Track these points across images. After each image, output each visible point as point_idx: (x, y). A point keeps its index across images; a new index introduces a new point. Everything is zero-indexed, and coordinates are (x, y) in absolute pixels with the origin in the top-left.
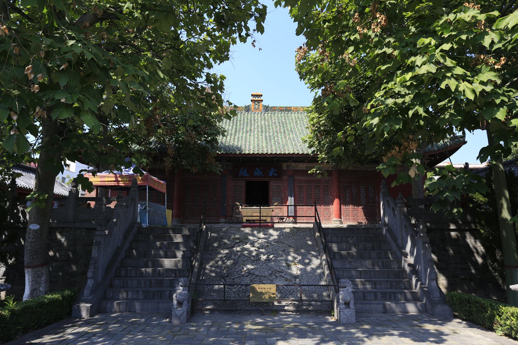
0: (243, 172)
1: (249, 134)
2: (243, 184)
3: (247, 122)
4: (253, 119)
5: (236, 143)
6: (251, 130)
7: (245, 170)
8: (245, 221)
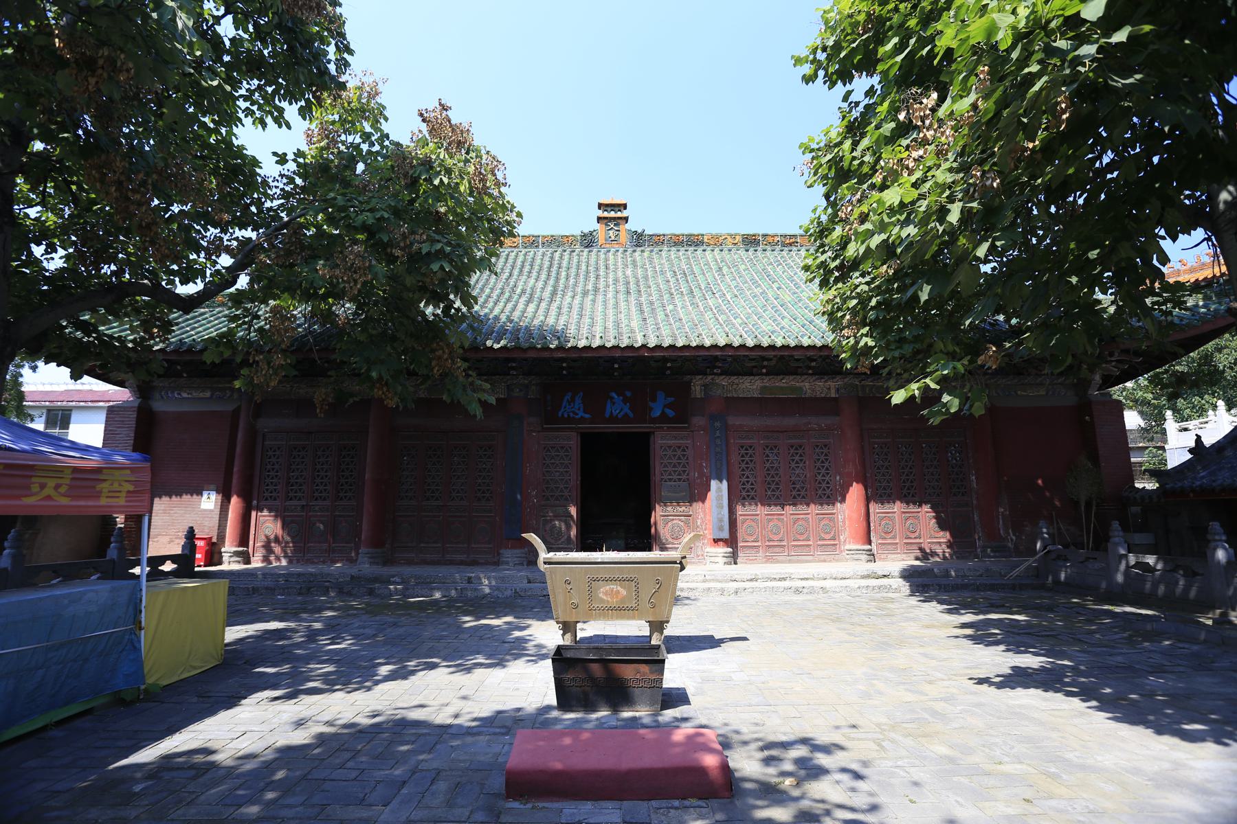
1: (591, 297)
2: (572, 441)
3: (587, 272)
4: (601, 263)
5: (551, 321)
6: (596, 290)
7: (578, 401)
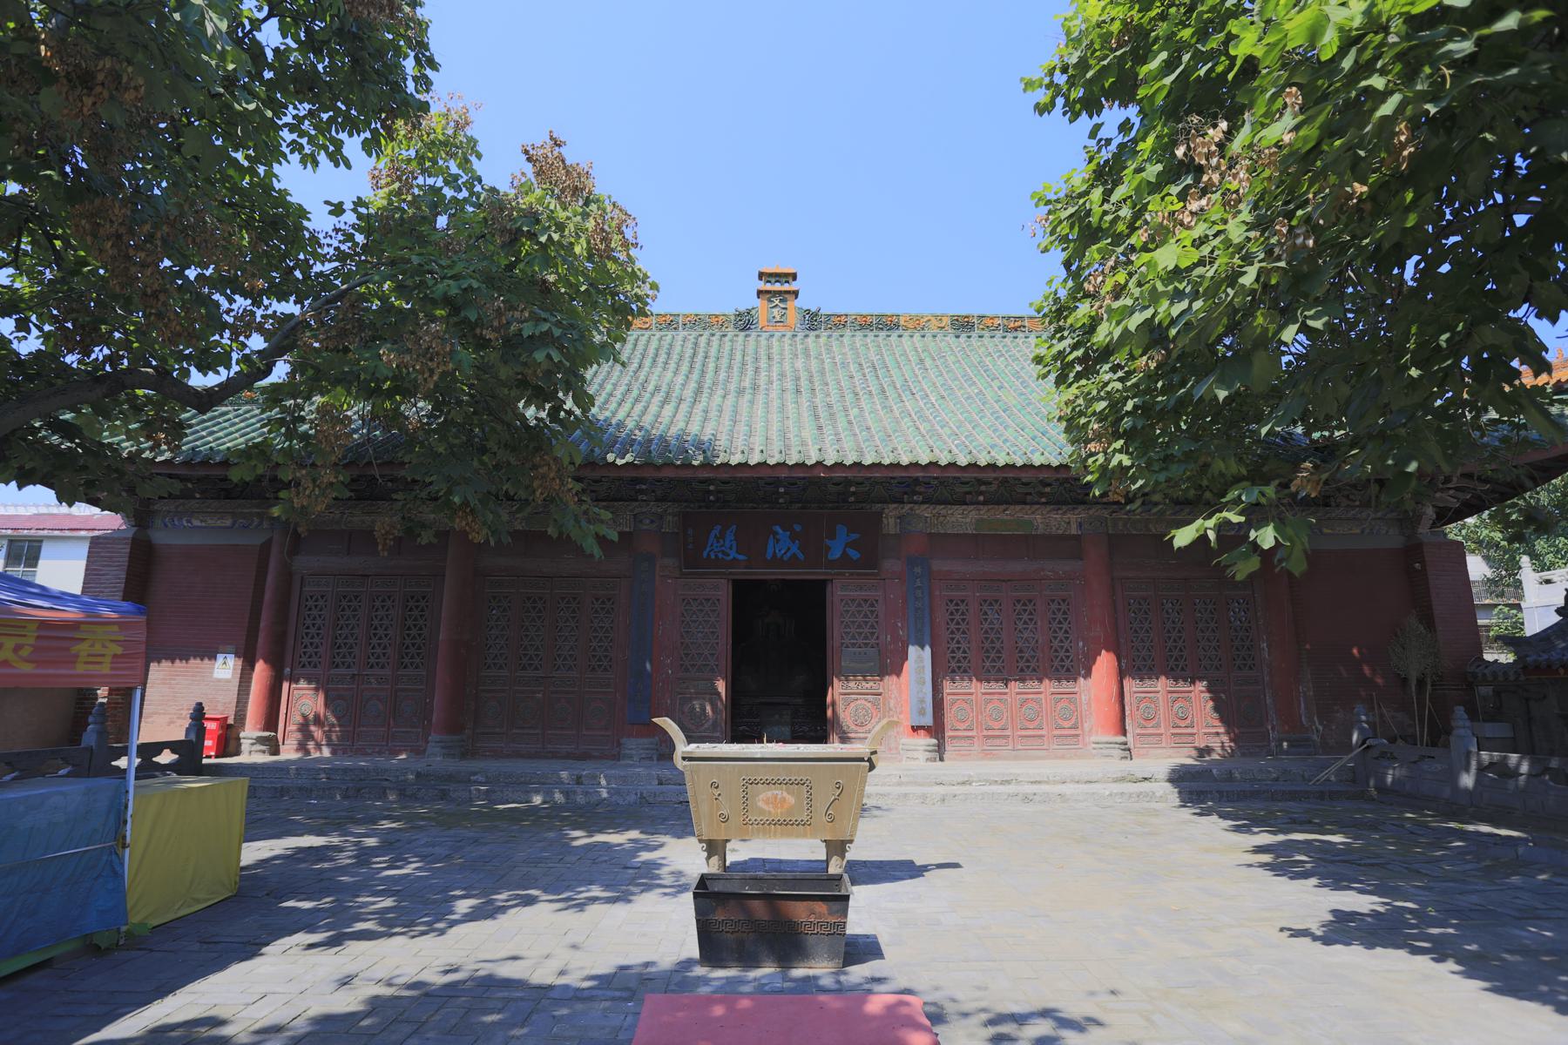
0: (724, 544)
2: (722, 593)
5: (694, 429)
6: (755, 387)
7: (730, 536)
8: (715, 860)
